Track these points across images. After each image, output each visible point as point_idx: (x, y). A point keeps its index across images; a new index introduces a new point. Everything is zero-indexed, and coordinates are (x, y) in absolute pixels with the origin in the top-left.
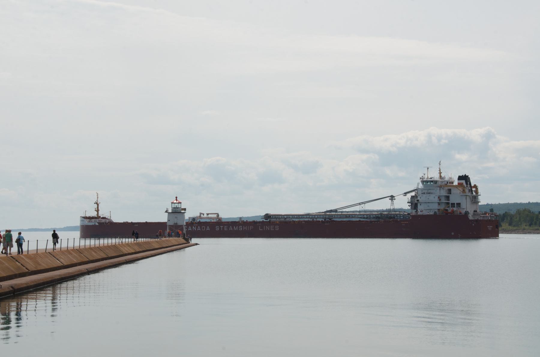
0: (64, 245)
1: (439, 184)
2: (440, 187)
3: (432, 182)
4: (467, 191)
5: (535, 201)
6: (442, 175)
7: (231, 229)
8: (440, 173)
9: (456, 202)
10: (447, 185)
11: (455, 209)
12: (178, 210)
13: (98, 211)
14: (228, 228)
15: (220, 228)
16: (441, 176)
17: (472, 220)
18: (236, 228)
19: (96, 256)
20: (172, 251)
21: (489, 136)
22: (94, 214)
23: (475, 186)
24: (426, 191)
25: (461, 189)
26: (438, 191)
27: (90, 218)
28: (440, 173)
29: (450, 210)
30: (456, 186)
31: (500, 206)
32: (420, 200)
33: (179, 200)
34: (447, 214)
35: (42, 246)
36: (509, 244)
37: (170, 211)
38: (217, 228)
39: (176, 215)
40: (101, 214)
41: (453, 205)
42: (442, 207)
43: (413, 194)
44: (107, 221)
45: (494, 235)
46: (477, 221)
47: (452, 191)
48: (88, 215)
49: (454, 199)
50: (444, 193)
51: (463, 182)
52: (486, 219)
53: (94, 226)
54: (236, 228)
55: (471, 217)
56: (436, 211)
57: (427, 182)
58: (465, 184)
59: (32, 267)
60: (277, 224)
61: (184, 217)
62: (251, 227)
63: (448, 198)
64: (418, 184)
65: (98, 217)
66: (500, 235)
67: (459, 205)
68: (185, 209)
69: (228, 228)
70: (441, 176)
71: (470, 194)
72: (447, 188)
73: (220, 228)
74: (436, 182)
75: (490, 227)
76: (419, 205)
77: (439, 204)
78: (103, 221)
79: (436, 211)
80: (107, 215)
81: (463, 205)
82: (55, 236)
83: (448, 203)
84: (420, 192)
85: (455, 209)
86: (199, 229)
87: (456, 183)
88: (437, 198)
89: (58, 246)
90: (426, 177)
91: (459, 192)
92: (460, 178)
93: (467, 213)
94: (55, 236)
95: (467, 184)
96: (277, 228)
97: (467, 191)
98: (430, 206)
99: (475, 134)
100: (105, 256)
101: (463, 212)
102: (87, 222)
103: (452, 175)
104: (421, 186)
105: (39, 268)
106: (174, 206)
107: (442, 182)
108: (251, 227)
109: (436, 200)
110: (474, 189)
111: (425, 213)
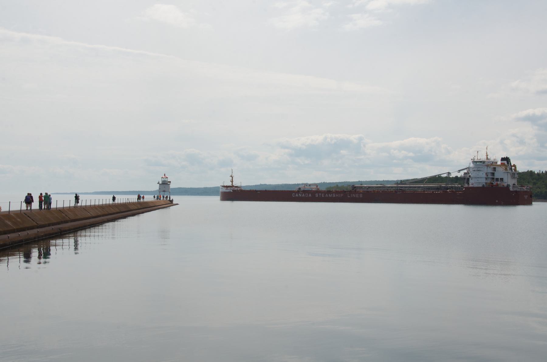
0: (84, 204)
1: (486, 163)
2: (487, 166)
3: (481, 162)
4: (508, 169)
5: (387, 180)
6: (489, 157)
7: (327, 196)
8: (487, 155)
9: (499, 177)
10: (492, 165)
11: (499, 183)
12: (166, 182)
13: (232, 182)
14: (325, 195)
15: (319, 195)
16: (487, 158)
17: (512, 191)
18: (330, 196)
19: (113, 211)
20: (159, 209)
21: (361, 139)
22: (230, 184)
23: (514, 166)
24: (476, 169)
25: (503, 167)
26: (486, 169)
27: (227, 187)
28: (487, 155)
29: (495, 183)
30: (499, 165)
31: (366, 182)
32: (472, 176)
33: (166, 176)
34: (492, 186)
35: (67, 205)
36: (540, 209)
37: (161, 183)
38: (317, 195)
39: (164, 185)
40: (234, 184)
41: (497, 179)
42: (489, 181)
43: (466, 171)
44: (239, 189)
45: (529, 203)
46: (516, 192)
47: (497, 169)
48: (225, 185)
49: (497, 176)
50: (490, 170)
51: (505, 162)
52: (522, 190)
53: (230, 192)
54: (330, 196)
55: (511, 189)
56: (484, 184)
57: (476, 162)
58: (506, 163)
59: (72, 217)
60: (361, 193)
61: (169, 187)
62: (342, 195)
63: (493, 174)
64: (470, 163)
65: (232, 186)
66: (533, 203)
67: (502, 179)
68: (170, 182)
69: (325, 195)
70: (487, 158)
71: (510, 171)
72: (492, 167)
73: (319, 195)
74: (484, 162)
75: (526, 197)
76: (470, 179)
77: (486, 179)
78: (236, 189)
79: (484, 184)
80: (239, 185)
81: (505, 180)
82: (77, 198)
83: (493, 178)
84: (471, 170)
85: (499, 183)
86: (303, 195)
87: (499, 163)
88: (485, 174)
89: (79, 205)
90: (476, 158)
91: (502, 169)
92: (503, 159)
93: (508, 186)
94: (77, 198)
95: (508, 163)
96: (361, 196)
97: (508, 169)
98: (478, 180)
99: (354, 138)
100: (118, 211)
101: (505, 185)
102: (224, 190)
103: (497, 157)
104: (472, 165)
105: (77, 218)
106: (163, 180)
107: (489, 162)
108: (342, 195)
109: (484, 175)
110: (513, 168)
111: (476, 185)
